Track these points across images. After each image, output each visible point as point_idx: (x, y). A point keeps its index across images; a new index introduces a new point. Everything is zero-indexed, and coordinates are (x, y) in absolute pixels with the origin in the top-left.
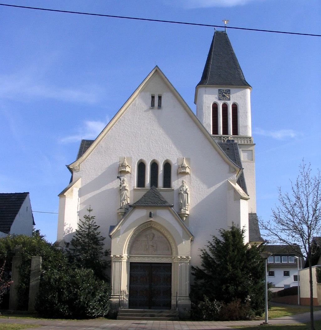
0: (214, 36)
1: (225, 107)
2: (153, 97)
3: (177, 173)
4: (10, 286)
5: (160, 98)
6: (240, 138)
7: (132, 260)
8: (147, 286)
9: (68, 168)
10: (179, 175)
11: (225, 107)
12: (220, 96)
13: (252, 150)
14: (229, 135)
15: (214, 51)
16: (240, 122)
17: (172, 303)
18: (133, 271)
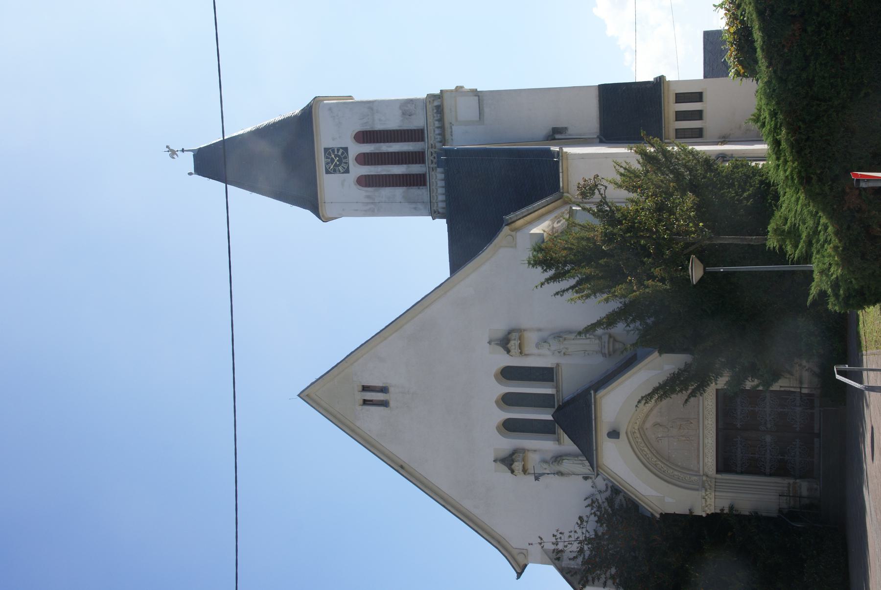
2: (366, 402)
5: (365, 389)
12: (339, 171)
14: (424, 127)
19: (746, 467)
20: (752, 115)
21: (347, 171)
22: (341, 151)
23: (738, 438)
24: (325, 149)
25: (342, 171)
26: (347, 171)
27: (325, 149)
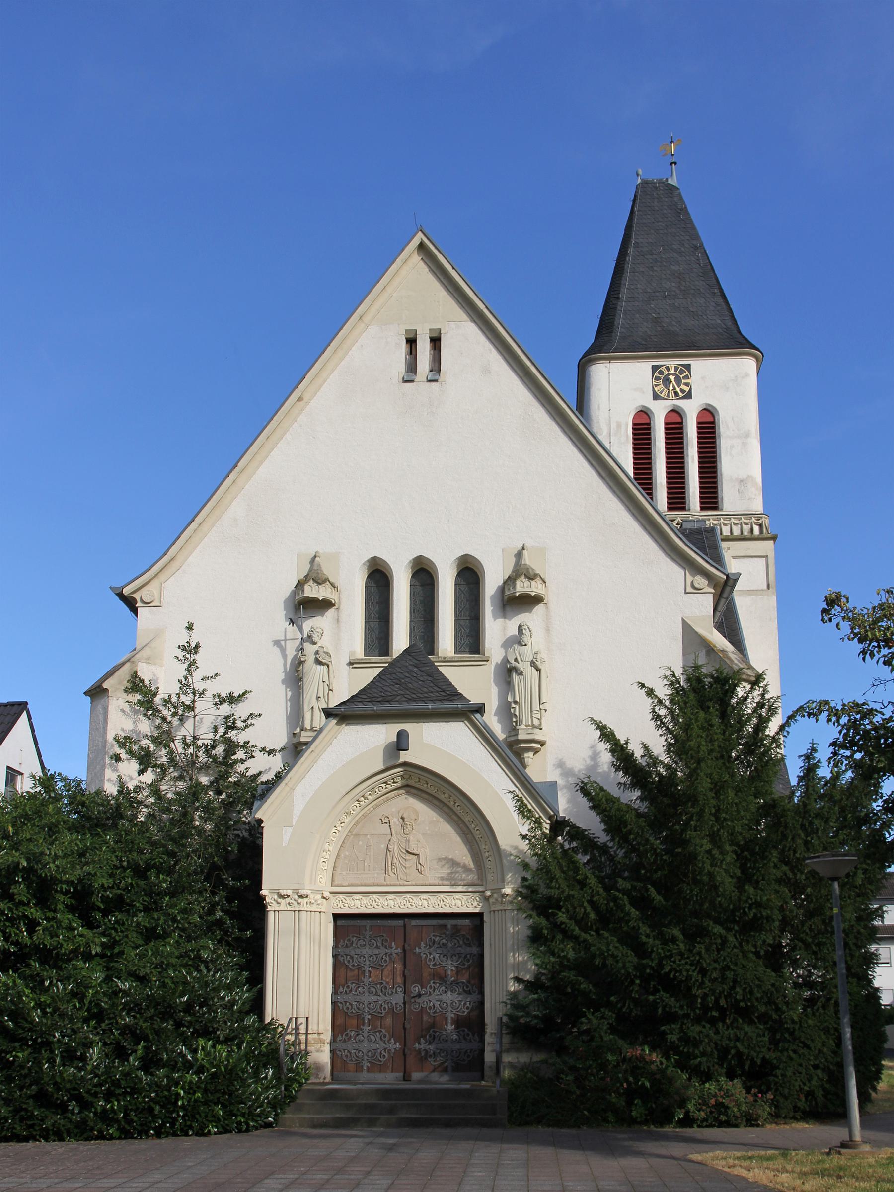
0: (635, 196)
1: (675, 430)
2: (412, 342)
3: (503, 600)
4: (832, 837)
5: (436, 342)
6: (728, 516)
7: (374, 904)
8: (398, 999)
9: (121, 596)
10: (508, 608)
11: (675, 430)
12: (656, 386)
13: (767, 556)
14: (689, 510)
15: (635, 242)
16: (634, 1159)
17: (486, 1060)
18: (347, 946)
19: (346, 962)
20: (512, 846)
21: (656, 397)
22: (687, 389)
23: (397, 949)
24: (689, 365)
25: (656, 389)
26: (656, 397)
27: (689, 365)
